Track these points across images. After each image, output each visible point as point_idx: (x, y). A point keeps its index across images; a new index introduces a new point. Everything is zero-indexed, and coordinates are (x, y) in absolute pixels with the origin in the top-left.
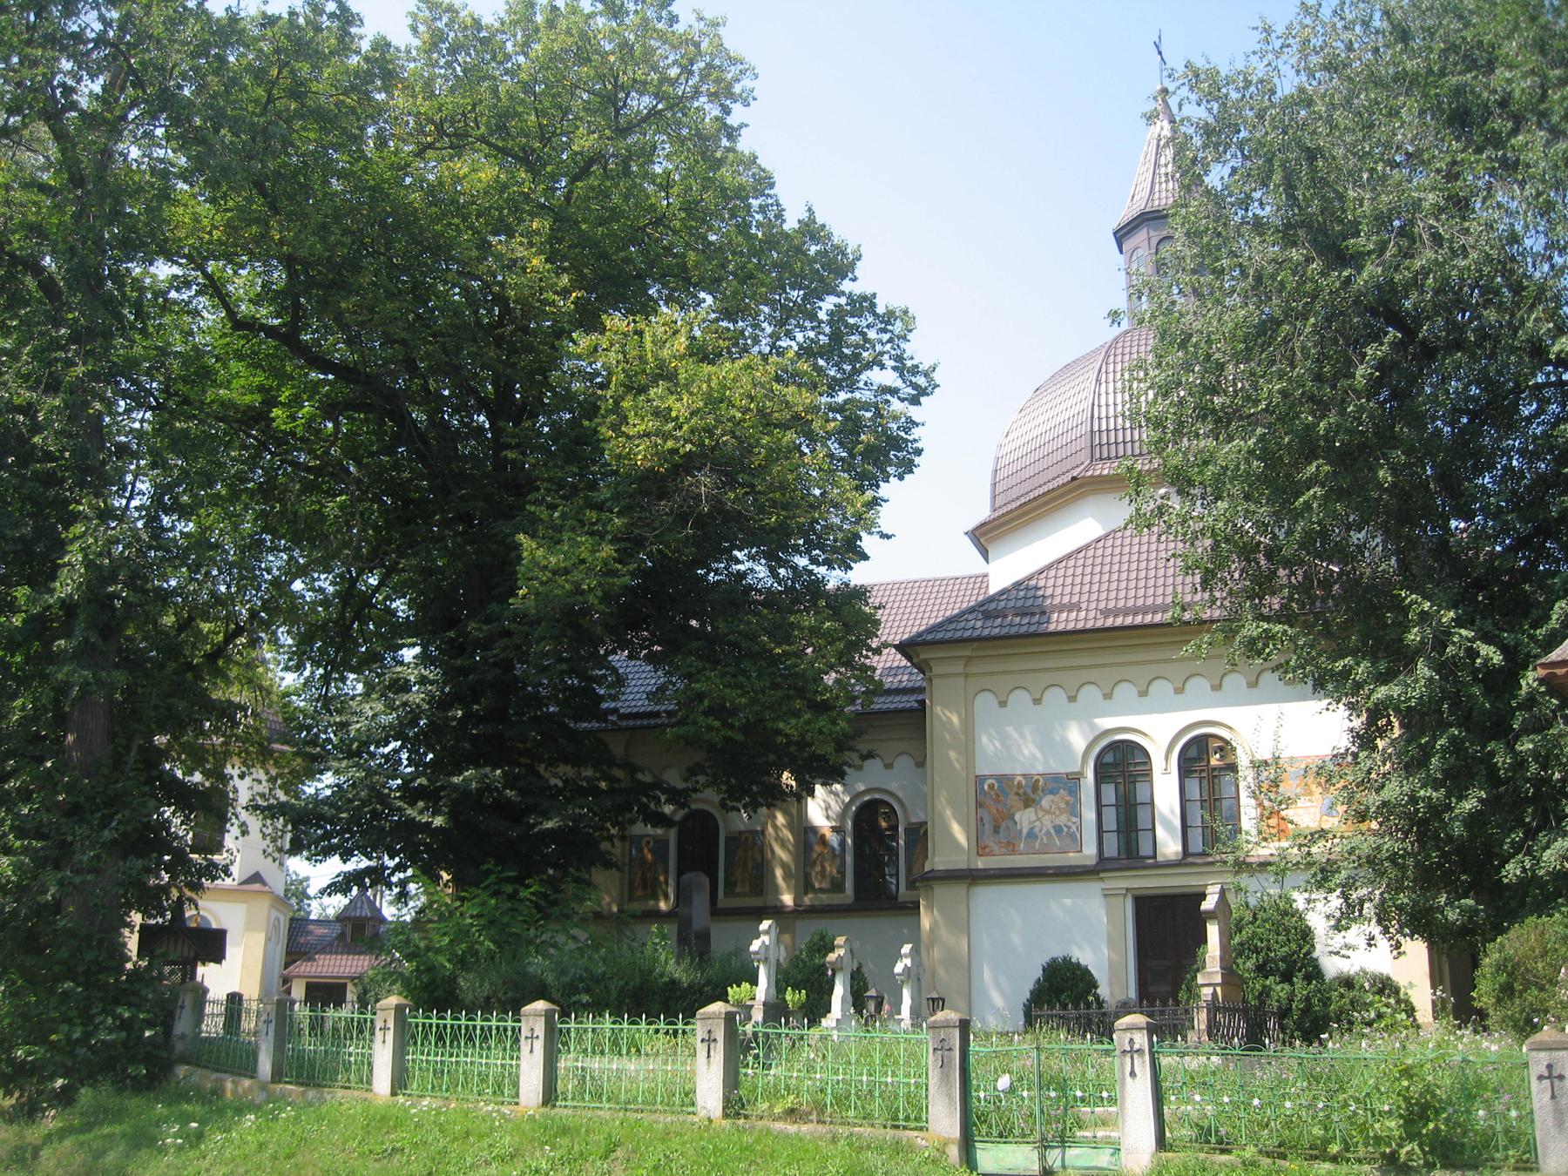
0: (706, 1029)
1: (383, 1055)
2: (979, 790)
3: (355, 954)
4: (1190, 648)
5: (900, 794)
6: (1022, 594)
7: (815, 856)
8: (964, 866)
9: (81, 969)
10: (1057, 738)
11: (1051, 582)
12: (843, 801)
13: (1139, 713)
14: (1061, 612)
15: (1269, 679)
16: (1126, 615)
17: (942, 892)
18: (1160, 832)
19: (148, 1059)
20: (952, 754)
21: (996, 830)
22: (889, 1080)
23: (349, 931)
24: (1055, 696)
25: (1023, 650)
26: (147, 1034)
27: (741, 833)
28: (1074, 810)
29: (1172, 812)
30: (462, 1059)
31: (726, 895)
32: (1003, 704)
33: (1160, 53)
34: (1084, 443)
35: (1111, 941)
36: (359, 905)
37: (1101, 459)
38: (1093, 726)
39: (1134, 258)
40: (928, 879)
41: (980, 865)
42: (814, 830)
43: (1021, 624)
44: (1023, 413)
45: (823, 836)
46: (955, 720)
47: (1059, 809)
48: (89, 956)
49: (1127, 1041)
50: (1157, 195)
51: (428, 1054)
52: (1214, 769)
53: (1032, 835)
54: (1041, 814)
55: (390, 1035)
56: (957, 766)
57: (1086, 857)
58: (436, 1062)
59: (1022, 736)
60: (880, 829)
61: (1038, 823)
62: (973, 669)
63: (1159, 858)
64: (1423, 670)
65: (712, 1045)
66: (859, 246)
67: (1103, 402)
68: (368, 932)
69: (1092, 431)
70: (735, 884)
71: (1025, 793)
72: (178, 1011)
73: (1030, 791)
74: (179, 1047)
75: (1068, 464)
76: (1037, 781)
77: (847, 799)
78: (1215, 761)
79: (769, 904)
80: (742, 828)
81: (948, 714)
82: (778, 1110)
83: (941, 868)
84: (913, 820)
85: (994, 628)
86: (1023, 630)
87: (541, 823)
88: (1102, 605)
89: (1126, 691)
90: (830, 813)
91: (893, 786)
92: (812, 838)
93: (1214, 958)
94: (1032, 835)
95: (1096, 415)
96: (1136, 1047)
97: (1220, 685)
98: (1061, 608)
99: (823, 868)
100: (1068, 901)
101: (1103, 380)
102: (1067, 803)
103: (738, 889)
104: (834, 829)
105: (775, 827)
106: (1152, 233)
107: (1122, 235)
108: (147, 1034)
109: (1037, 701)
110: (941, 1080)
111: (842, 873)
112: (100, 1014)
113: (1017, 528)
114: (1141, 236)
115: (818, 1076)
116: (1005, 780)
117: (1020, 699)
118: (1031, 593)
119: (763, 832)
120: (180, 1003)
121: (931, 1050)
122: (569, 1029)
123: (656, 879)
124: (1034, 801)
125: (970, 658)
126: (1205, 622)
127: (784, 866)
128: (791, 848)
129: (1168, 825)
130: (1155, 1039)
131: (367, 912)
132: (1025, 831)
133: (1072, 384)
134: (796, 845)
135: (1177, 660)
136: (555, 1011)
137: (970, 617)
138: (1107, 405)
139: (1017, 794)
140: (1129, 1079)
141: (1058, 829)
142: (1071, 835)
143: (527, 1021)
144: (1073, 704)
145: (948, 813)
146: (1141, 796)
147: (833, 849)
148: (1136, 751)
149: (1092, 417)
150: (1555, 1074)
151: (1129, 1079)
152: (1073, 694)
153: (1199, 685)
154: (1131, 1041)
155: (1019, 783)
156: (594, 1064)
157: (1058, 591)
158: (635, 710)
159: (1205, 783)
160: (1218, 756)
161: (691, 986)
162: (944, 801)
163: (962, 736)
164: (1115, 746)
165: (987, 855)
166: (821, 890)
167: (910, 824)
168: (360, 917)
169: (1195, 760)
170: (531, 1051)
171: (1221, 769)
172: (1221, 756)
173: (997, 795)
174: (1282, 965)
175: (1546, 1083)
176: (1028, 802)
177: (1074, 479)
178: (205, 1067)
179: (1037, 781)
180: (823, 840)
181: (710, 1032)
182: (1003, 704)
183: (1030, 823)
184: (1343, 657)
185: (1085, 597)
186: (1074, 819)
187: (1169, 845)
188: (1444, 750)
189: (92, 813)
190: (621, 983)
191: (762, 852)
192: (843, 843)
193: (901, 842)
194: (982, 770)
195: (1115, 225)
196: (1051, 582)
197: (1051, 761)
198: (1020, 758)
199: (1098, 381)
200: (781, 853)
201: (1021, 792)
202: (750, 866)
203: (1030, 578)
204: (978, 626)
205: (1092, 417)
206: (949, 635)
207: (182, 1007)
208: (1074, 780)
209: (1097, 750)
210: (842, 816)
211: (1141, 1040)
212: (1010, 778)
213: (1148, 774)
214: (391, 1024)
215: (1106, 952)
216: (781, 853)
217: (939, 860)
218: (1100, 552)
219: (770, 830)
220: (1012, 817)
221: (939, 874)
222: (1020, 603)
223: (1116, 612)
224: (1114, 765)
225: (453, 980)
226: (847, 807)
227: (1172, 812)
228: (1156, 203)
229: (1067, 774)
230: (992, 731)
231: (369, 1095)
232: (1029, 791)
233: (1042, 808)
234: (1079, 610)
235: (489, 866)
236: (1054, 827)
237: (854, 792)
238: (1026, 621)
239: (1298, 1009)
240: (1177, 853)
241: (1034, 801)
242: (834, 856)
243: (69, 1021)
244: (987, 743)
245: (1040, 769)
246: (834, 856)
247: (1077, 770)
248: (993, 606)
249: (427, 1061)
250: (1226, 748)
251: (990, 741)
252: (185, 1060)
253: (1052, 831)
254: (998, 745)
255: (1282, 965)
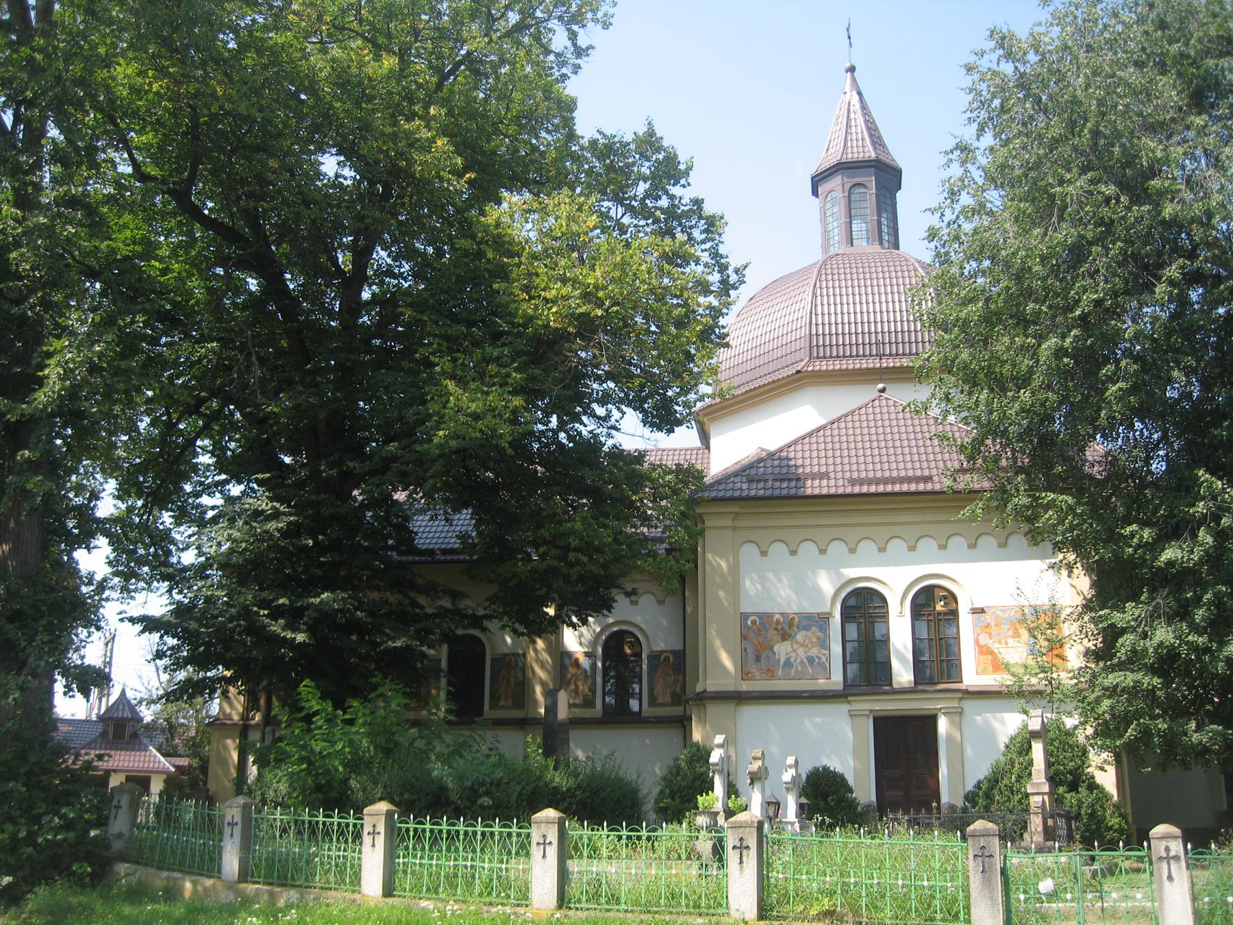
0: (737, 837)
1: (372, 859)
2: (743, 625)
3: (127, 750)
4: (966, 512)
5: (643, 626)
6: (776, 463)
7: (569, 676)
8: (732, 689)
9: (23, 770)
10: (810, 584)
11: (799, 455)
12: (594, 631)
13: (879, 565)
14: (813, 479)
15: (1019, 541)
16: (885, 483)
17: (713, 710)
18: (895, 664)
19: (90, 857)
20: (721, 594)
21: (758, 659)
22: (926, 883)
23: (111, 730)
24: (808, 549)
25: (768, 510)
26: (92, 834)
27: (505, 655)
28: (824, 644)
29: (905, 647)
30: (461, 862)
31: (491, 708)
32: (793, 553)
33: (849, 37)
34: (804, 343)
35: (856, 754)
36: (121, 707)
37: (818, 358)
38: (840, 575)
39: (829, 198)
40: (701, 699)
41: (744, 688)
42: (569, 654)
43: (784, 488)
44: (741, 317)
45: (577, 660)
46: (724, 564)
47: (812, 643)
48: (33, 758)
49: (1162, 849)
50: (850, 150)
51: (421, 858)
52: (939, 614)
53: (788, 663)
54: (796, 646)
55: (381, 840)
56: (726, 603)
57: (836, 683)
58: (339, 857)
59: (780, 581)
60: (626, 655)
61: (793, 654)
62: (739, 524)
63: (895, 685)
64: (1205, 537)
65: (745, 852)
66: (692, 157)
67: (819, 312)
68: (129, 731)
69: (810, 334)
70: (499, 698)
71: (782, 629)
72: (113, 811)
73: (787, 627)
74: (117, 846)
75: (789, 360)
76: (793, 619)
77: (598, 629)
78: (939, 607)
79: (529, 716)
80: (506, 651)
81: (718, 559)
82: (814, 912)
83: (712, 690)
84: (655, 649)
85: (757, 490)
86: (785, 492)
87: (386, 642)
88: (847, 475)
89: (867, 547)
90: (583, 640)
91: (638, 620)
92: (567, 661)
93: (1039, 771)
94: (788, 663)
95: (814, 322)
96: (1172, 853)
97: (975, 545)
98: (813, 477)
99: (577, 686)
100: (818, 720)
101: (818, 293)
102: (818, 638)
103: (501, 703)
104: (587, 654)
105: (536, 650)
106: (846, 180)
107: (817, 181)
108: (92, 834)
109: (793, 553)
110: (984, 884)
111: (593, 691)
112: (46, 813)
113: (730, 414)
114: (836, 182)
115: (852, 880)
116: (765, 617)
117: (778, 550)
118: (785, 462)
119: (524, 655)
120: (115, 803)
121: (971, 856)
122: (458, 832)
123: (429, 693)
124: (790, 635)
125: (737, 514)
126: (978, 492)
127: (543, 684)
128: (549, 668)
129: (902, 658)
130: (1189, 846)
131: (127, 714)
132: (782, 660)
133: (788, 296)
134: (554, 666)
135: (955, 521)
136: (395, 811)
137: (736, 480)
138: (823, 314)
139: (775, 629)
140: (1166, 883)
141: (811, 660)
142: (821, 665)
143: (539, 828)
144: (911, 553)
145: (718, 643)
146: (879, 632)
147: (585, 671)
148: (875, 597)
149: (811, 323)
150: (744, 845)
151: (1166, 883)
152: (884, 545)
153: (927, 545)
154: (1167, 849)
155: (778, 622)
156: (595, 867)
157: (808, 462)
158: (449, 546)
159: (932, 624)
160: (942, 603)
161: (569, 790)
162: (714, 633)
163: (730, 579)
164: (858, 592)
165: (751, 679)
166: (661, 705)
167: (652, 652)
168: (122, 718)
169: (923, 605)
170: (544, 856)
171: (945, 614)
172: (945, 604)
173: (759, 630)
174: (1069, 777)
175: (371, 836)
176: (785, 636)
177: (798, 372)
178: (146, 865)
179: (793, 619)
180: (576, 663)
181: (374, 826)
182: (764, 553)
183: (787, 654)
184: (1130, 524)
185: (831, 468)
186: (824, 652)
187: (903, 674)
188: (1210, 603)
189: (35, 620)
190: (519, 788)
191: (524, 674)
192: (594, 666)
193: (645, 667)
194: (746, 608)
195: (812, 171)
196: (799, 455)
197: (805, 604)
198: (779, 599)
199: (814, 294)
200: (541, 673)
201: (779, 627)
202: (513, 684)
203: (781, 450)
204: (743, 489)
205: (811, 323)
206: (721, 494)
207: (118, 807)
208: (824, 619)
209: (843, 595)
210: (593, 644)
211: (1176, 847)
212: (770, 615)
213: (885, 616)
214: (381, 828)
215: (852, 763)
216: (541, 673)
217: (711, 683)
218: (836, 432)
219: (532, 652)
220: (771, 648)
221: (708, 695)
222: (777, 470)
223: (861, 482)
224: (857, 607)
225: (345, 781)
226: (599, 635)
227: (905, 647)
228: (850, 156)
229: (818, 614)
230: (754, 575)
231: (357, 896)
232: (786, 627)
233: (797, 642)
234: (829, 479)
235: (378, 680)
236: (807, 658)
237: (604, 624)
238: (785, 485)
239: (1087, 814)
240: (910, 682)
241: (790, 635)
242: (587, 677)
243: (12, 820)
244: (750, 586)
245: (795, 609)
246: (587, 677)
247: (826, 611)
248: (753, 472)
249: (421, 865)
250: (951, 597)
251: (752, 584)
252: (123, 858)
253: (805, 661)
254: (759, 587)
255: (1069, 777)
